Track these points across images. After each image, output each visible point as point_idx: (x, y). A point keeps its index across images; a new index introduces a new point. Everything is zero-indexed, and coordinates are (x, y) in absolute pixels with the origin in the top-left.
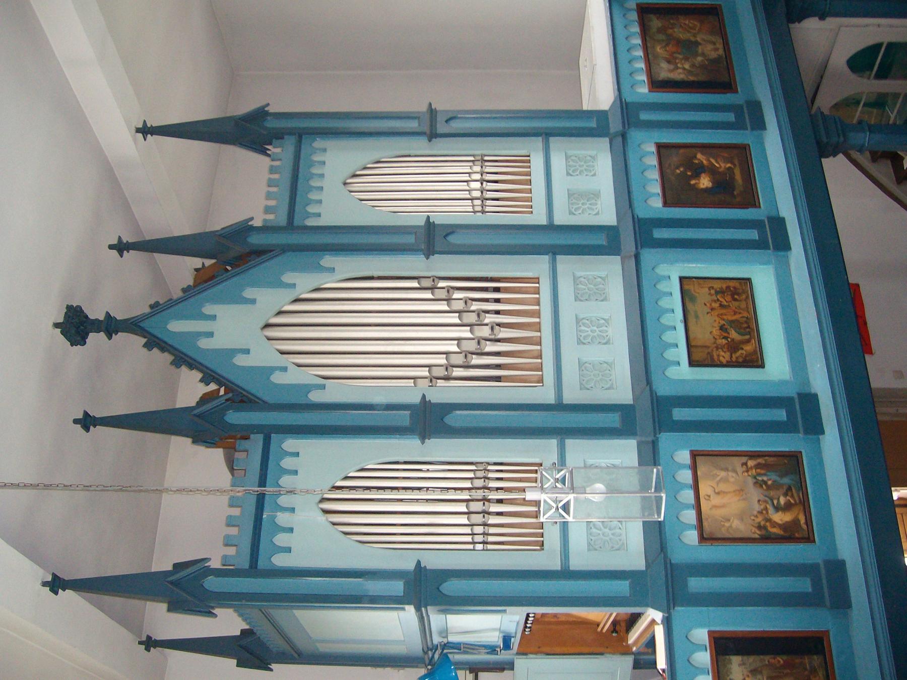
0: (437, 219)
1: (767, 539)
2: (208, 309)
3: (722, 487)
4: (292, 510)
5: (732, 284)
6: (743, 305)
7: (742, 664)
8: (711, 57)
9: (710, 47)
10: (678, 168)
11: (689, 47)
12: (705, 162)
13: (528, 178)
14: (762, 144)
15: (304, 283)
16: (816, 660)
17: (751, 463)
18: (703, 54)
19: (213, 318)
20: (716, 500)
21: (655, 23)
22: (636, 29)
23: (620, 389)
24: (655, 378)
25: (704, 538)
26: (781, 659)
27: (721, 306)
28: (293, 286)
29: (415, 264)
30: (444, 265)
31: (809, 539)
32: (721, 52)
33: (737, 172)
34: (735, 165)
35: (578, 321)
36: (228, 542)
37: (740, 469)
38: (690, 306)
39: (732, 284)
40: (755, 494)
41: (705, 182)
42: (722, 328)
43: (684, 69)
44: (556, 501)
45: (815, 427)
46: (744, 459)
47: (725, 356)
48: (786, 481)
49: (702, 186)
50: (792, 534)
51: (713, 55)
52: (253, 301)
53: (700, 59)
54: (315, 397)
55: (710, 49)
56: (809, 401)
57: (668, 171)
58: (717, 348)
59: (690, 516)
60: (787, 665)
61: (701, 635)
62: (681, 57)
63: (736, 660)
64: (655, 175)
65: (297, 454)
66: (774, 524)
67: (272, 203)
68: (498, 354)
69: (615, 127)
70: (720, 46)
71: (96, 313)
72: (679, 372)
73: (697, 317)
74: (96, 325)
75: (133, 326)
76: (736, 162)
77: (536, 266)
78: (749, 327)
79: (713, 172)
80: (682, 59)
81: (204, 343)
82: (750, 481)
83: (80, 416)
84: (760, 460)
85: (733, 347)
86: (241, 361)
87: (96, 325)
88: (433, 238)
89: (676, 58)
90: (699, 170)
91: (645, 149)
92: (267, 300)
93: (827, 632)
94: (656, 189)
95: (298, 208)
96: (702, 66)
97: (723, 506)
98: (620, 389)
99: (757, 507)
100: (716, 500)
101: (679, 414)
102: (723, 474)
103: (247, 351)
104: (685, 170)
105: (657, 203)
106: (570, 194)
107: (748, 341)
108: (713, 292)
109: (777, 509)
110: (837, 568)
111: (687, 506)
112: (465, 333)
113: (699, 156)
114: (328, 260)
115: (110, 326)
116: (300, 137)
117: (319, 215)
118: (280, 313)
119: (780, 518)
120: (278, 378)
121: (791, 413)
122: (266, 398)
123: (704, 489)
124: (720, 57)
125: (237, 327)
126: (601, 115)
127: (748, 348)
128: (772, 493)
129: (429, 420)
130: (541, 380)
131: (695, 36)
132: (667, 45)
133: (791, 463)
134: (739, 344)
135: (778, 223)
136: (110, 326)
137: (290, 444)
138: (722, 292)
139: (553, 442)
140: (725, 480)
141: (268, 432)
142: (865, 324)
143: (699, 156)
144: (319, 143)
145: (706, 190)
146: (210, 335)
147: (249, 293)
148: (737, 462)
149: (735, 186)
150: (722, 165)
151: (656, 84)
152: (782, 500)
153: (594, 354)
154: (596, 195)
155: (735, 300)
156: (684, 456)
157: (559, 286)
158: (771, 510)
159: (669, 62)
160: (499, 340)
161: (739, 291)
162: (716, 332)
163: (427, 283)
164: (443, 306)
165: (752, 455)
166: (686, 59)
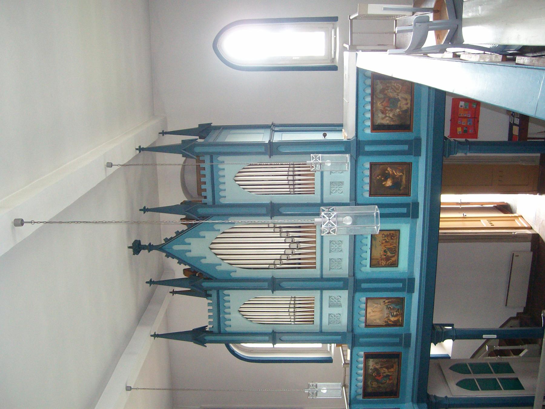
0: (274, 202)
1: (388, 325)
2: (187, 240)
3: (375, 309)
4: (230, 314)
5: (392, 232)
6: (395, 241)
7: (373, 361)
8: (403, 109)
9: (404, 102)
10: (378, 176)
13: (314, 239)
14: (418, 162)
16: (396, 360)
17: (386, 301)
19: (190, 244)
20: (372, 314)
23: (344, 270)
24: (357, 271)
25: (367, 326)
26: (385, 360)
27: (386, 242)
28: (219, 230)
30: (279, 220)
31: (401, 325)
32: (409, 105)
34: (403, 174)
35: (331, 242)
37: (382, 304)
38: (374, 242)
39: (392, 232)
40: (386, 311)
41: (389, 183)
42: (385, 251)
43: (389, 117)
44: (316, 157)
45: (411, 290)
46: (384, 300)
47: (384, 263)
48: (398, 307)
50: (396, 324)
51: (405, 107)
52: (204, 237)
53: (398, 110)
54: (233, 275)
56: (412, 281)
57: (374, 178)
58: (381, 260)
59: (364, 318)
60: (387, 361)
61: (362, 353)
62: (389, 109)
63: (371, 360)
64: (367, 180)
65: (229, 295)
66: (391, 321)
68: (300, 254)
69: (356, 148)
70: (409, 101)
71: (145, 242)
72: (366, 269)
73: (376, 247)
74: (144, 247)
75: (160, 248)
76: (404, 173)
78: (395, 251)
79: (393, 177)
80: (389, 111)
81: (188, 254)
82: (385, 307)
83: (149, 280)
84: (390, 300)
85: (388, 259)
86: (203, 261)
87: (144, 247)
88: (273, 210)
89: (386, 110)
90: (386, 176)
91: (365, 164)
92: (209, 236)
94: (367, 188)
96: (399, 116)
97: (375, 316)
98: (344, 270)
99: (386, 316)
100: (372, 314)
101: (364, 286)
102: (376, 305)
103: (205, 258)
104: (381, 178)
105: (367, 195)
106: (331, 183)
107: (393, 256)
109: (393, 316)
110: (409, 336)
111: (363, 303)
112: (287, 246)
113: (389, 169)
114: (231, 220)
115: (150, 248)
119: (393, 319)
120: (218, 268)
121: (404, 285)
122: (215, 276)
123: (369, 310)
124: (408, 108)
125: (198, 248)
127: (393, 259)
128: (392, 311)
129: (275, 285)
130: (315, 268)
133: (400, 301)
134: (390, 258)
135: (416, 205)
136: (150, 248)
137: (221, 158)
138: (387, 236)
139: (319, 291)
140: (376, 307)
141: (218, 289)
142: (478, 121)
143: (389, 169)
145: (389, 187)
146: (190, 251)
147: (202, 233)
148: (382, 301)
149: (402, 188)
150: (398, 174)
151: (376, 128)
152: (395, 313)
153: (336, 256)
154: (342, 183)
155: (392, 239)
156: (364, 299)
158: (390, 316)
159: (383, 113)
160: (300, 249)
161: (395, 235)
162: (382, 253)
164: (278, 235)
165: (387, 298)
166: (391, 110)
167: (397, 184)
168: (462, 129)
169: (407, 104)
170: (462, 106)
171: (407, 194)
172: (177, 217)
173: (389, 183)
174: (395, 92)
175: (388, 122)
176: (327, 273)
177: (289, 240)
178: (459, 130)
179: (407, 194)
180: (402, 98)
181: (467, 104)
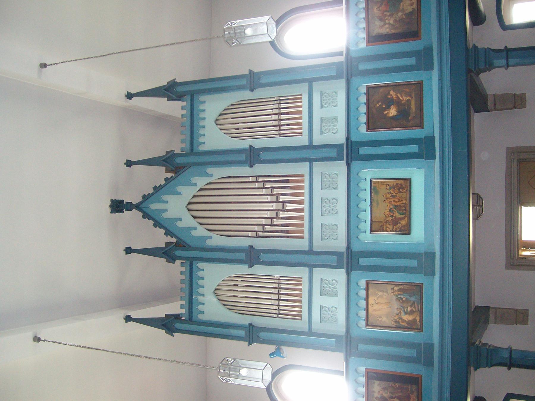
2: (165, 198)
8: (407, 12)
18: (403, 10)
29: (245, 170)
30: (260, 169)
32: (415, 6)
33: (413, 103)
43: (389, 24)
49: (391, 115)
51: (409, 9)
53: (400, 14)
62: (388, 14)
76: (413, 96)
77: (302, 168)
79: (398, 103)
104: (382, 105)
105: (363, 129)
108: (388, 187)
113: (392, 92)
114: (210, 170)
118: (194, 196)
126: (339, 254)
132: (381, 5)
143: (392, 92)
144: (202, 98)
147: (180, 189)
150: (404, 98)
154: (336, 119)
159: (381, 20)
163: (254, 179)
166: (391, 15)
169: (412, 4)
175: (388, 30)
176: (318, 140)
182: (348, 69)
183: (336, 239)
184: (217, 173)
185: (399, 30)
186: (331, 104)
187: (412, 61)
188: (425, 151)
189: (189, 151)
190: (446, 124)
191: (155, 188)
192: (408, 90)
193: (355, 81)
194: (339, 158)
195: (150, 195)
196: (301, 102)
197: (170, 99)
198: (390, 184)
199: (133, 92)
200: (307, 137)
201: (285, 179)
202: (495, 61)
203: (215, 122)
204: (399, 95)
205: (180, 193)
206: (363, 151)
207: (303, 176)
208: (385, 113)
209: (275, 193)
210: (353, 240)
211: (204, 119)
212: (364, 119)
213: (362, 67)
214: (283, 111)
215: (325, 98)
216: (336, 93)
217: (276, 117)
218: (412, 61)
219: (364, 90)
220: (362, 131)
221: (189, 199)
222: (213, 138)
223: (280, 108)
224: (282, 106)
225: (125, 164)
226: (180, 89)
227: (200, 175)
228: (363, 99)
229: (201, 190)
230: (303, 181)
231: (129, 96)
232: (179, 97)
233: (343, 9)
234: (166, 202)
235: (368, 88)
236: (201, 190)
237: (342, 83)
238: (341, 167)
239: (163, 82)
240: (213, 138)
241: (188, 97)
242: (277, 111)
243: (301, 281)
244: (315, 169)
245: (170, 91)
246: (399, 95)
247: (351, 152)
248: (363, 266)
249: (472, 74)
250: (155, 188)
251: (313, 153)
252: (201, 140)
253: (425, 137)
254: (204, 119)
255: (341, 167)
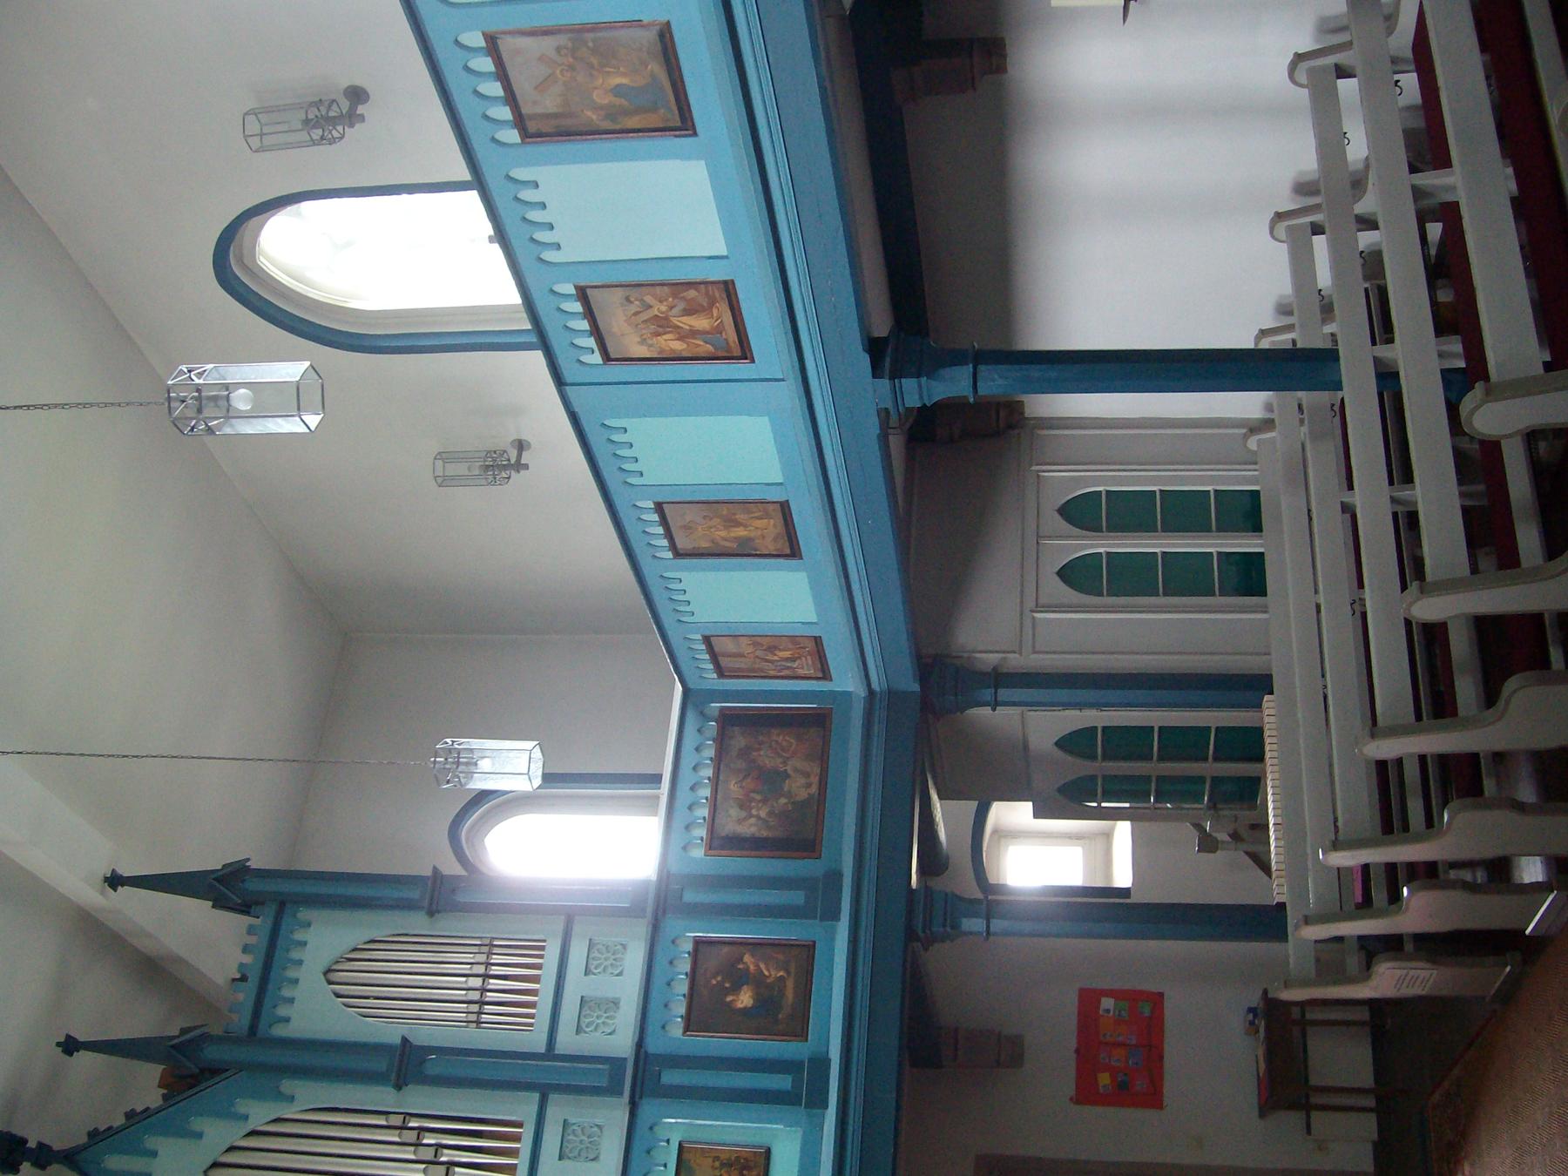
2: (151, 1142)
8: (798, 799)
9: (802, 781)
11: (770, 781)
12: (752, 967)
15: (260, 1114)
18: (789, 795)
21: (739, 740)
22: (710, 752)
28: (246, 1118)
29: (380, 1096)
30: (418, 1099)
32: (814, 789)
33: (790, 984)
34: (788, 973)
36: (246, 949)
43: (759, 818)
49: (740, 1005)
51: (803, 794)
53: (783, 801)
55: (800, 787)
62: (758, 797)
67: (252, 940)
70: (815, 780)
76: (793, 971)
77: (522, 1108)
79: (758, 982)
90: (738, 979)
93: (819, 857)
95: (278, 954)
104: (723, 981)
105: (676, 1030)
108: (717, 1164)
113: (747, 958)
114: (287, 1085)
116: (282, 904)
117: (287, 1020)
118: (232, 1149)
124: (811, 797)
126: (616, 1063)
131: (785, 763)
132: (745, 777)
143: (747, 958)
144: (304, 914)
147: (197, 1124)
150: (772, 973)
154: (615, 1003)
157: (545, 1137)
159: (741, 807)
163: (396, 1120)
166: (765, 801)
167: (768, 1003)
168: (1114, 1078)
169: (809, 785)
170: (1108, 1011)
171: (801, 1034)
172: (154, 1071)
173: (745, 999)
174: (780, 756)
175: (753, 829)
176: (567, 1041)
177: (410, 1136)
178: (1104, 1079)
179: (801, 1034)
180: (796, 770)
181: (1124, 1004)
182: (661, 905)
183: (620, 974)
184: (308, 1095)
185: (779, 833)
186: (610, 970)
187: (797, 898)
188: (803, 1092)
189: (245, 1031)
190: (854, 1070)
191: (130, 1115)
192: (781, 957)
193: (673, 925)
194: (613, 1090)
195: (111, 1131)
196: (541, 957)
197: (220, 903)
198: (723, 1156)
199: (81, 1039)
200: (546, 1028)
201: (473, 1128)
202: (964, 920)
203: (325, 974)
204: (762, 966)
205: (199, 1136)
206: (670, 1077)
207: (520, 1125)
208: (729, 999)
209: (443, 1159)
210: (653, 1027)
211: (300, 962)
212: (681, 1009)
213: (690, 897)
214: (496, 970)
215: (596, 954)
216: (624, 947)
217: (477, 982)
218: (797, 898)
219: (689, 947)
220: (673, 1034)
221: (215, 1154)
222: (311, 1009)
223: (488, 964)
224: (495, 959)
225: (58, 1044)
226: (253, 885)
227: (259, 1095)
228: (685, 966)
229: (254, 1133)
230: (516, 1138)
231: (114, 881)
232: (245, 908)
233: (657, 798)
234: (154, 1154)
235: (698, 942)
236: (254, 1133)
237: (642, 929)
238: (610, 1118)
239: (212, 861)
240: (311, 1009)
241: (270, 910)
242: (481, 969)
243: (543, 948)
244: (551, 1111)
245: (227, 887)
246: (762, 966)
247: (642, 1079)
248: (671, 1087)
249: (917, 945)
250: (130, 1115)
251: (549, 1075)
252: (282, 1011)
253: (810, 1060)
254: (300, 962)
255: (610, 1118)
